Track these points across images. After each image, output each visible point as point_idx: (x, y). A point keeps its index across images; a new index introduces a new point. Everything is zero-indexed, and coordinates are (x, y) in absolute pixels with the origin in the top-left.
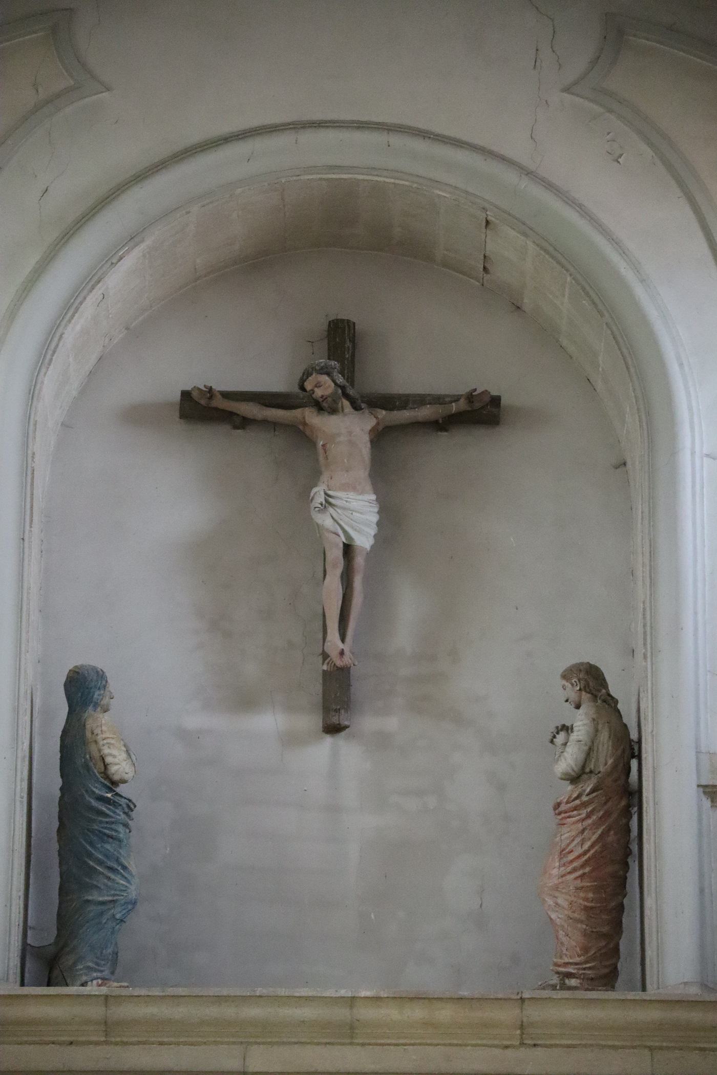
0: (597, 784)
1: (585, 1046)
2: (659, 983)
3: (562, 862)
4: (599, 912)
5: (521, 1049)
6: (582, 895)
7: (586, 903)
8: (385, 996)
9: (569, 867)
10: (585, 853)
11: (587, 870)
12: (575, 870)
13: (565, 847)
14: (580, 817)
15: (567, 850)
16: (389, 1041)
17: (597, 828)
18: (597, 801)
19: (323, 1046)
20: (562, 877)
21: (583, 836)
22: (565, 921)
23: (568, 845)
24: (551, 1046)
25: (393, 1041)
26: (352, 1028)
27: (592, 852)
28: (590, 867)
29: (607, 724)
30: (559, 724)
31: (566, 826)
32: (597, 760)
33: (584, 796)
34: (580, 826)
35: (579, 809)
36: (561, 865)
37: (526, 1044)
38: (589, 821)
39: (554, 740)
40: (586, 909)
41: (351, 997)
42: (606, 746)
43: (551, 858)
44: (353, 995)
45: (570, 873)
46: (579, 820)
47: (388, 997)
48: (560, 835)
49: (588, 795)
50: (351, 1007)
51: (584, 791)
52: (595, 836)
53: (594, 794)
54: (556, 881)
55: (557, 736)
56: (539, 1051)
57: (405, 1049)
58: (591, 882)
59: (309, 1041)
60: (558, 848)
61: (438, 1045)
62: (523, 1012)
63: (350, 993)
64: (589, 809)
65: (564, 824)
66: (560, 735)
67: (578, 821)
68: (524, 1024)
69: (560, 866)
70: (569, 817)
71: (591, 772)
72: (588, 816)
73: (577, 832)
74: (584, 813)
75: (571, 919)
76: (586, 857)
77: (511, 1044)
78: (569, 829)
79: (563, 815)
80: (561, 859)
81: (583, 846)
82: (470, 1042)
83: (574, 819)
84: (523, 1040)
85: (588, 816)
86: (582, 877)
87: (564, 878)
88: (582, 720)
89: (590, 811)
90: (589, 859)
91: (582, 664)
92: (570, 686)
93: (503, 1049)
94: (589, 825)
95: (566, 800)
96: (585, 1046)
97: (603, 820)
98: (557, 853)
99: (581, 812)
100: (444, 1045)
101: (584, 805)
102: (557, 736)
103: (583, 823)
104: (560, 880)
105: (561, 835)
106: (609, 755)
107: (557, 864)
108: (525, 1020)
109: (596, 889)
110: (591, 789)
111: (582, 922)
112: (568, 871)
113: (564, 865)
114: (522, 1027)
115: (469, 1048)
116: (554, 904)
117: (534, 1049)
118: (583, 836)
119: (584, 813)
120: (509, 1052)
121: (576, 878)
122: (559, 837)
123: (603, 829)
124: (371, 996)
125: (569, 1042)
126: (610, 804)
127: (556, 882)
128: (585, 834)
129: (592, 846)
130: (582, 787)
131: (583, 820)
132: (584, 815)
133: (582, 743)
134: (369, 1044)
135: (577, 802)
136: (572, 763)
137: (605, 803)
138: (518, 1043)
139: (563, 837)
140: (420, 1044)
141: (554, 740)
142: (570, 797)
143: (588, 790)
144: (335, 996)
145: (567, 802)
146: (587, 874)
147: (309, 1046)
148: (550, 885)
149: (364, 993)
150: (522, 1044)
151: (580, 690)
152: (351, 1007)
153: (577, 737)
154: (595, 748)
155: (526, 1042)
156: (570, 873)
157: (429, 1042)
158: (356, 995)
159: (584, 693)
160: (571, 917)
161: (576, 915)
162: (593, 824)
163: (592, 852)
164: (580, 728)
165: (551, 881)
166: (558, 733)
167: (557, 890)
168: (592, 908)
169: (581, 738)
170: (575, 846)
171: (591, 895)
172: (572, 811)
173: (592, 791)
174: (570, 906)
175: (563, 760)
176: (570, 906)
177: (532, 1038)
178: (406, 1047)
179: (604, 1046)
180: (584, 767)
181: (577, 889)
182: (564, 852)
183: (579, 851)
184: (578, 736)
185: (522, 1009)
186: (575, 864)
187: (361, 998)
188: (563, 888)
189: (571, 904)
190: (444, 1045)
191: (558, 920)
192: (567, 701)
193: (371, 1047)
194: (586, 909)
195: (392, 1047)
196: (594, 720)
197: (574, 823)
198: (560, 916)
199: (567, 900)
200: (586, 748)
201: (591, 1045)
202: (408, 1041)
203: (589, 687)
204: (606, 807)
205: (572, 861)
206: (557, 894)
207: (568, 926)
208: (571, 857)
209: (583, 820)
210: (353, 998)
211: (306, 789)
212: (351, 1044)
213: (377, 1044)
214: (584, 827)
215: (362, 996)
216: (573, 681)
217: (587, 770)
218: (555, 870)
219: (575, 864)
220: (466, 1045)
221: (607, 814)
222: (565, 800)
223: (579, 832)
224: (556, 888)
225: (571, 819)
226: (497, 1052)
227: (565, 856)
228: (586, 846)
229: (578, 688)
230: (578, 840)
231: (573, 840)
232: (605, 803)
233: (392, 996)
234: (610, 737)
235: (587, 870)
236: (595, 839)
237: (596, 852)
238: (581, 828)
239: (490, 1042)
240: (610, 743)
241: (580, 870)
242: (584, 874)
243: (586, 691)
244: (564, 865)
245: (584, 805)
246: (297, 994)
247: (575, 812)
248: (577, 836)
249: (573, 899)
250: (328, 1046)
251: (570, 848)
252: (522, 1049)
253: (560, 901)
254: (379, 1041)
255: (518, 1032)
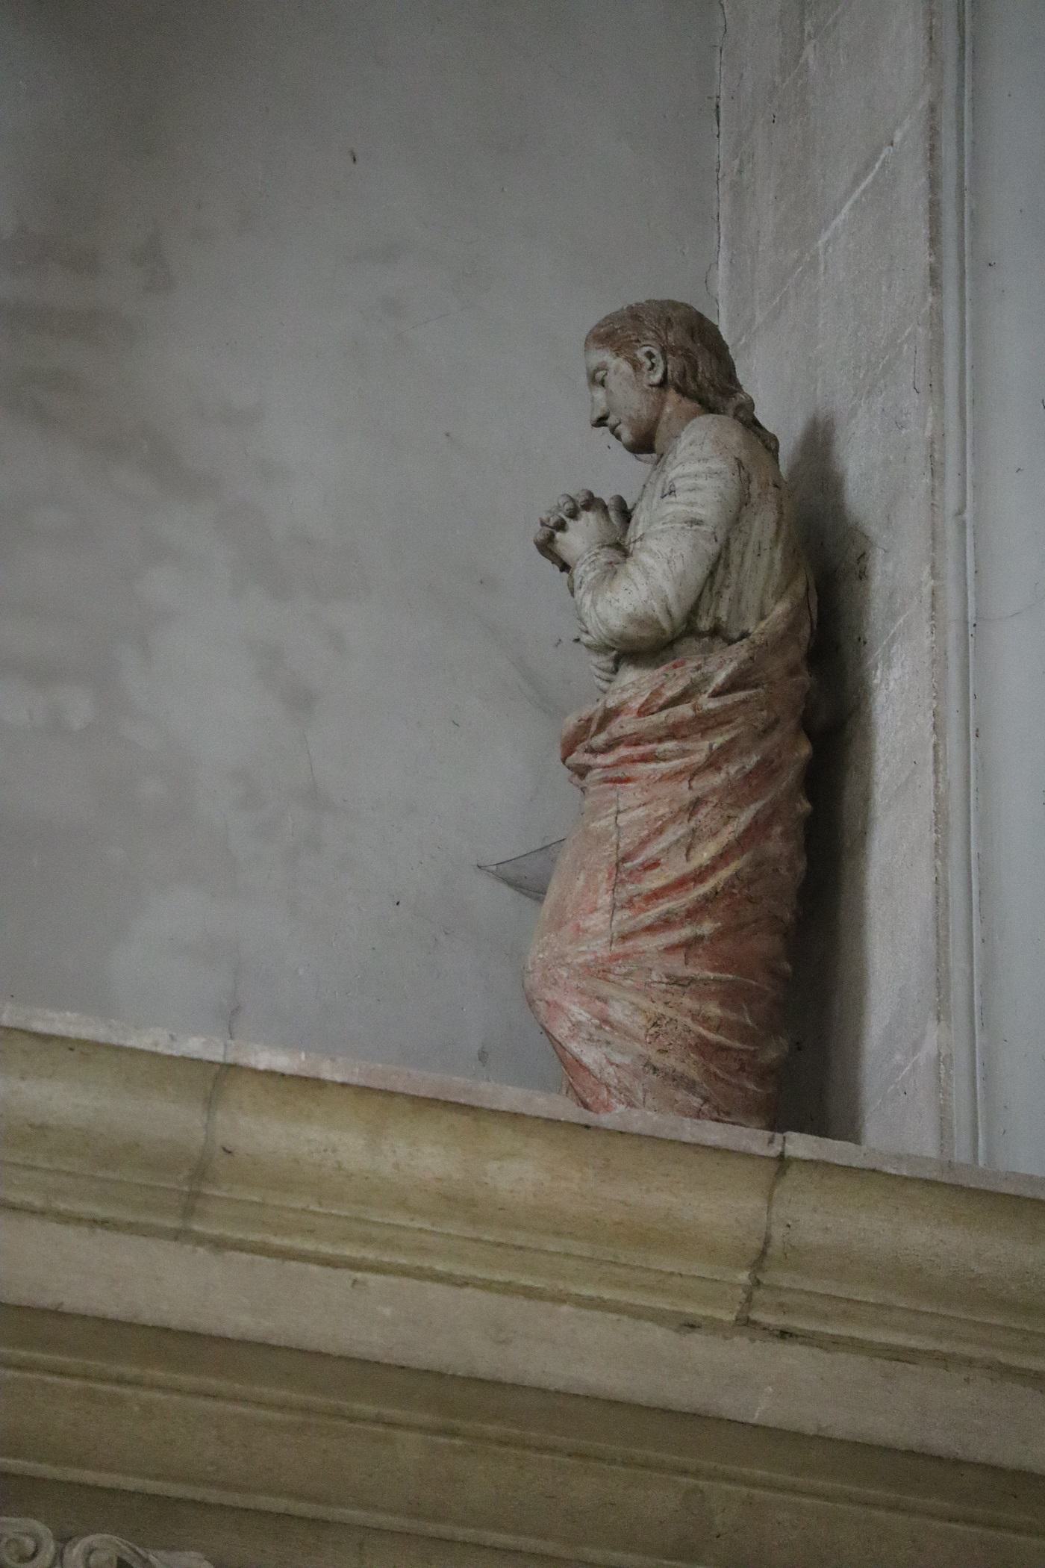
0: (750, 664)
1: (944, 1360)
2: (598, 1458)
3: (623, 894)
4: (736, 1066)
5: (736, 1339)
6: (688, 1002)
7: (704, 1032)
8: (339, 1078)
9: (644, 910)
10: (700, 876)
11: (707, 927)
12: (666, 923)
13: (631, 848)
14: (687, 760)
15: (639, 860)
16: (309, 1245)
17: (739, 804)
18: (740, 720)
19: (85, 1230)
20: (624, 938)
21: (692, 824)
22: (636, 1076)
23: (644, 843)
24: (835, 1343)
25: (327, 1249)
26: (201, 1172)
27: (724, 873)
28: (715, 921)
29: (772, 489)
30: (576, 490)
31: (630, 785)
32: (738, 598)
33: (706, 696)
34: (685, 792)
35: (684, 737)
36: (618, 904)
37: (755, 1323)
38: (717, 779)
39: (558, 535)
40: (702, 1047)
41: (222, 1065)
42: (765, 561)
43: (582, 877)
44: (230, 1060)
45: (650, 929)
46: (681, 772)
47: (344, 1085)
48: (614, 809)
49: (716, 694)
50: (210, 1103)
51: (707, 679)
52: (730, 828)
53: (740, 695)
54: (599, 948)
55: (570, 523)
56: (793, 1357)
57: (355, 1282)
58: (714, 969)
59: (39, 1203)
60: (608, 850)
61: (464, 1283)
62: (774, 1209)
63: (221, 1051)
64: (718, 741)
65: (628, 780)
66: (581, 522)
67: (677, 774)
68: (770, 1251)
69: (614, 907)
70: (645, 759)
71: (716, 632)
72: (713, 763)
73: (676, 807)
74: (702, 748)
75: (655, 1069)
76: (704, 888)
77: (705, 1318)
78: (646, 796)
79: (623, 751)
80: (619, 883)
81: (692, 853)
82: (574, 1290)
83: (663, 765)
84: (750, 1308)
85: (713, 763)
86: (688, 946)
87: (629, 944)
88: (706, 460)
89: (721, 747)
90: (708, 899)
91: (675, 305)
92: (626, 367)
93: (677, 1331)
94: (714, 791)
95: (642, 700)
96: (944, 1360)
97: (754, 782)
98: (604, 866)
99: (688, 745)
100: (487, 1286)
101: (704, 724)
102: (570, 523)
103: (694, 783)
104: (617, 949)
105: (618, 812)
106: (770, 590)
107: (605, 900)
108: (778, 1233)
109: (730, 996)
110: (729, 677)
111: (691, 1086)
112: (648, 922)
113: (630, 903)
114: (760, 1261)
115: (565, 1309)
116: (597, 1022)
117: (780, 1346)
118: (692, 824)
119: (702, 748)
120: (697, 1345)
121: (671, 949)
122: (612, 818)
123: (758, 812)
124: (288, 1072)
125: (899, 1339)
126: (776, 736)
127: (604, 953)
128: (700, 816)
129: (723, 857)
130: (698, 668)
131: (694, 773)
132: (699, 758)
133: (704, 528)
134: (240, 1246)
135: (685, 710)
136: (669, 589)
137: (767, 731)
138: (732, 1317)
139: (623, 820)
140: (404, 1272)
141: (558, 535)
142: (656, 693)
143: (720, 677)
144: (169, 1052)
145: (644, 711)
146: (706, 942)
147: (33, 1224)
148: (581, 960)
149: (265, 1059)
150: (745, 1323)
151: (663, 384)
152: (210, 1103)
153: (688, 509)
154: (736, 559)
155: (756, 1315)
156: (650, 929)
157: (440, 1267)
158: (243, 1061)
159: (672, 396)
160: (658, 1065)
161: (671, 1062)
162: (729, 788)
163: (724, 873)
164: (701, 482)
165: (583, 948)
166: (574, 515)
167: (606, 979)
168: (721, 1048)
169: (701, 512)
170: (667, 850)
171: (714, 1010)
172: (660, 740)
173: (732, 685)
174: (652, 1031)
175: (638, 577)
176: (652, 1031)
177: (781, 1305)
178: (359, 1275)
179: (1007, 1372)
180: (693, 613)
181: (675, 981)
182: (628, 865)
183: (677, 867)
184: (692, 504)
185: (770, 1199)
186: (665, 906)
187: (255, 1071)
188: (627, 975)
189: (655, 1024)
190: (487, 1286)
191: (611, 1070)
192: (601, 422)
193: (245, 1257)
194: (702, 1047)
195: (314, 1268)
196: (740, 464)
197: (666, 778)
198: (617, 1058)
199: (638, 1009)
200: (713, 548)
201: (970, 1362)
202: (370, 1255)
203: (694, 378)
204: (767, 744)
205: (656, 895)
206: (606, 989)
207: (645, 1091)
208: (654, 881)
209: (694, 773)
210: (230, 1070)
211: (506, 190)
212: (178, 1235)
213: (262, 1250)
214: (699, 794)
215: (262, 1067)
216: (640, 354)
217: (704, 624)
218: (596, 914)
219: (665, 906)
220: (560, 1299)
221: (766, 770)
222: (636, 705)
223: (680, 810)
224: (600, 971)
225: (652, 766)
226: (659, 1335)
227: (635, 875)
228: (705, 854)
229: (657, 378)
230: (677, 831)
231: (660, 831)
232: (767, 731)
233: (355, 1080)
234: (777, 533)
235: (707, 927)
236: (731, 837)
237: (737, 875)
238: (688, 796)
239: (641, 1300)
240: (778, 554)
241: (682, 925)
242: (698, 939)
243: (682, 391)
244: (630, 903)
245: (704, 724)
246: (39, 1027)
247: (670, 745)
248: (673, 819)
249: (661, 1009)
250: (99, 1231)
251: (652, 851)
252: (740, 1341)
253: (618, 1012)
254: (277, 1241)
255: (743, 1277)
